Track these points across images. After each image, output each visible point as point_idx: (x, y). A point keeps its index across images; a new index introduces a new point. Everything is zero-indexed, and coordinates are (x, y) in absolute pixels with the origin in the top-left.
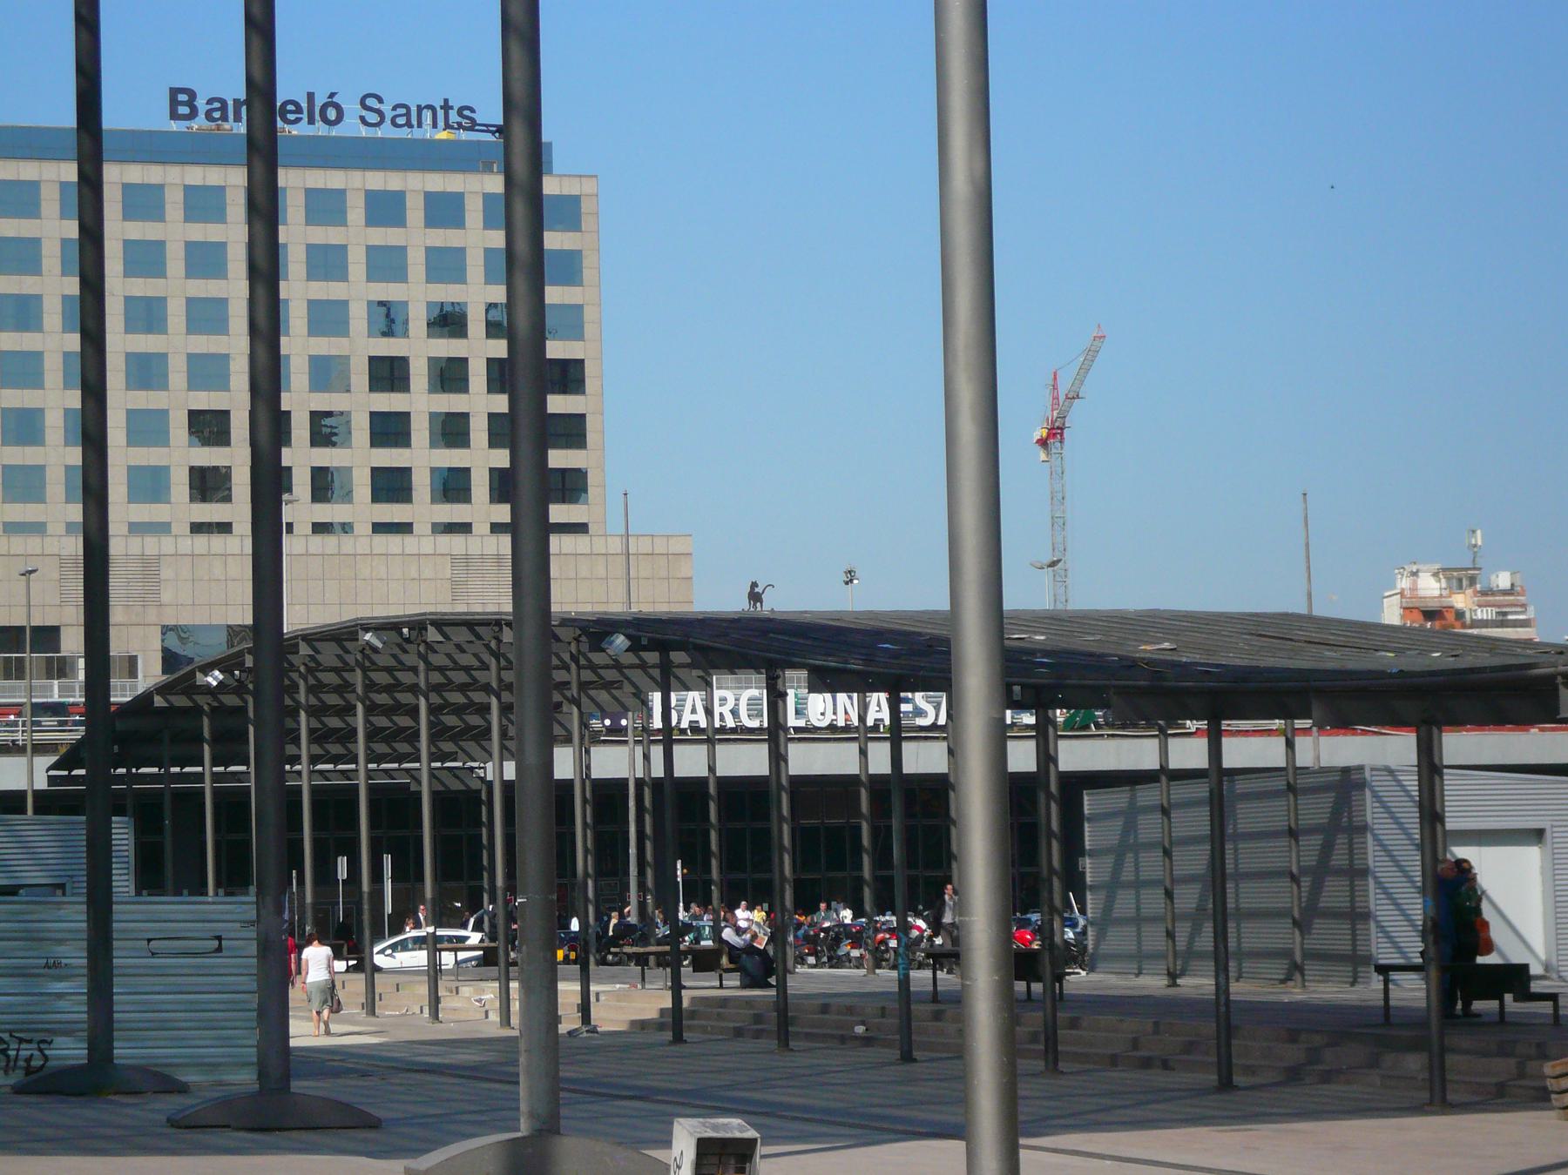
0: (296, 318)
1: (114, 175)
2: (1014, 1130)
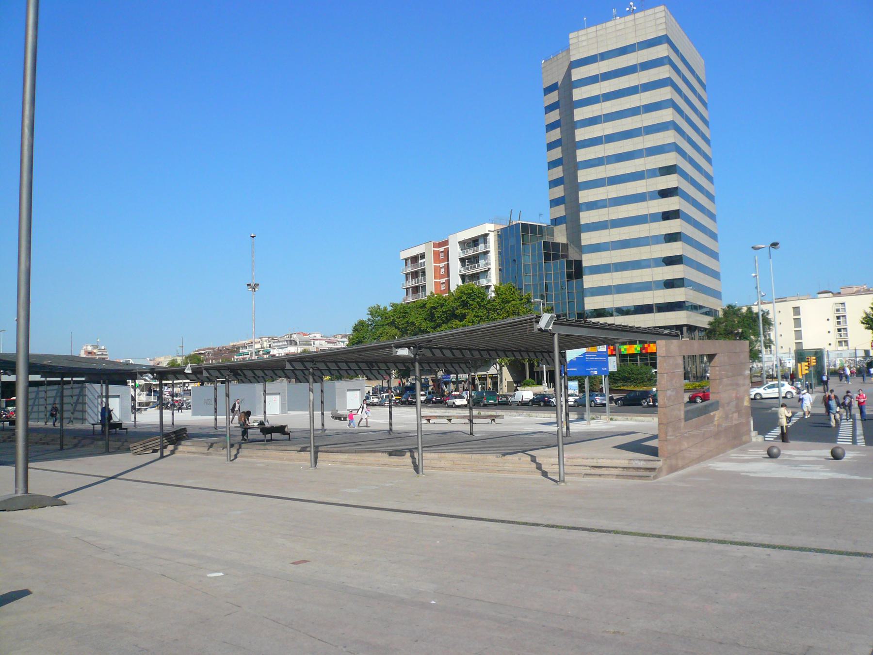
2: (27, 460)
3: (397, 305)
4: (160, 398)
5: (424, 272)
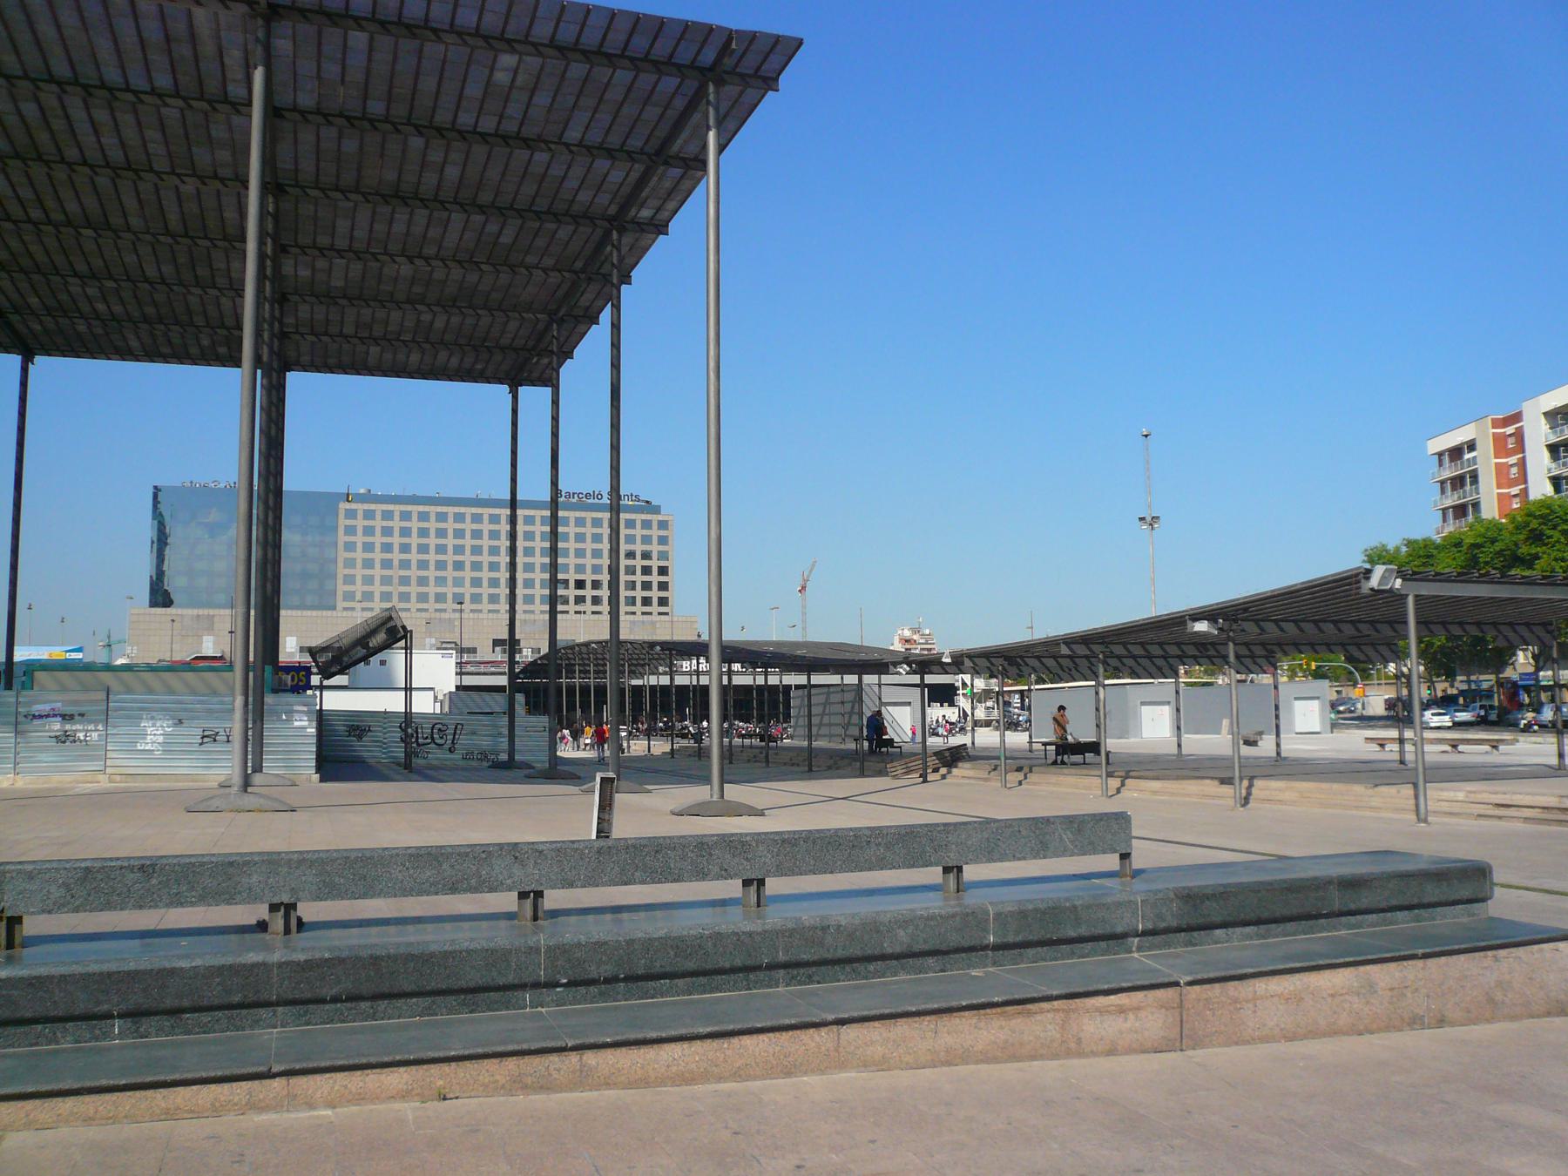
0: (504, 551)
1: (623, 516)
2: (722, 782)
3: (1416, 542)
4: (1007, 713)
5: (1474, 477)
